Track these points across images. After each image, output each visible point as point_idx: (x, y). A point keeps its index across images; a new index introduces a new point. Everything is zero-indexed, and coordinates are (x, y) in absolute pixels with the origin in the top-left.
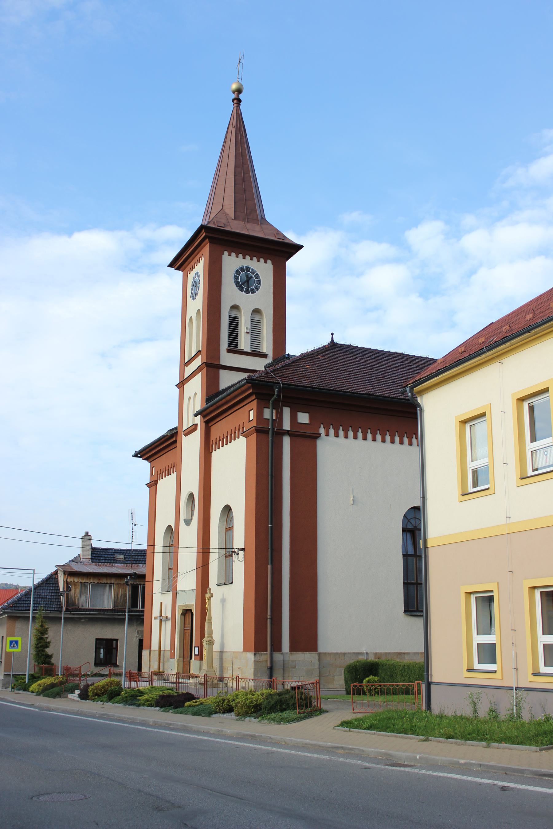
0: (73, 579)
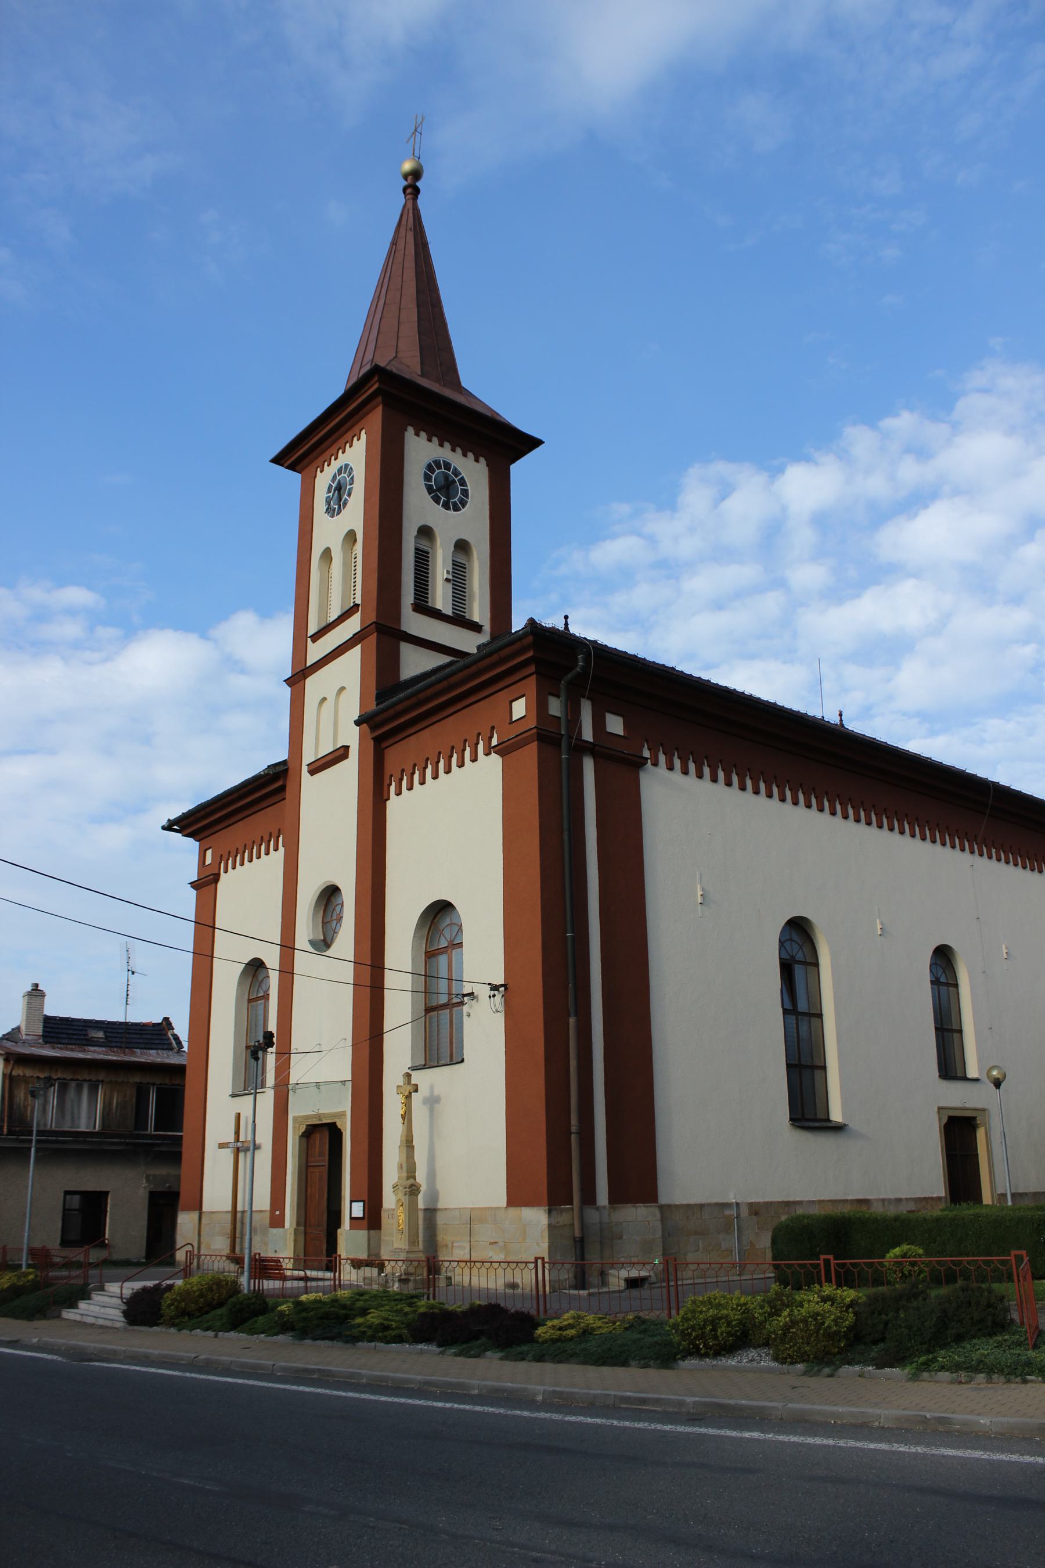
0: (23, 1071)
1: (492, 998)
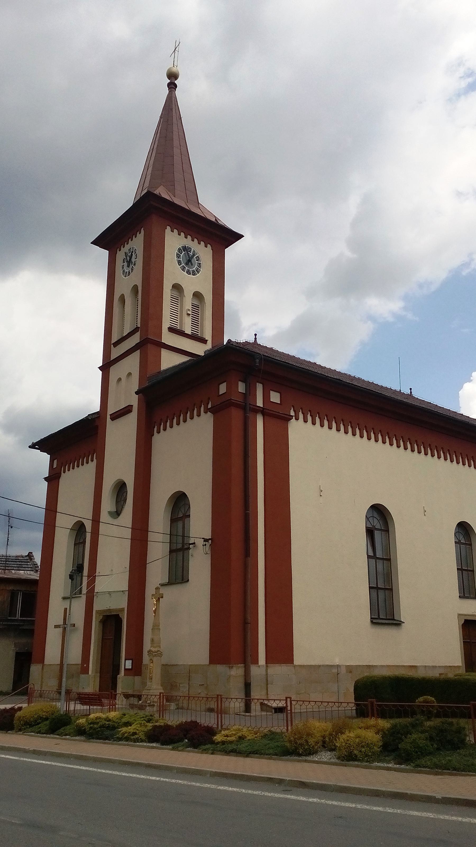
1: (204, 546)
